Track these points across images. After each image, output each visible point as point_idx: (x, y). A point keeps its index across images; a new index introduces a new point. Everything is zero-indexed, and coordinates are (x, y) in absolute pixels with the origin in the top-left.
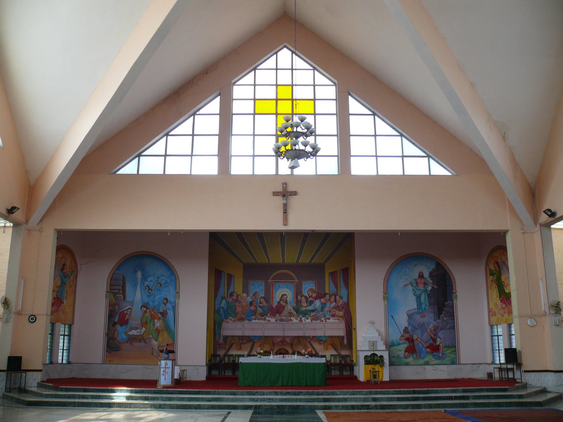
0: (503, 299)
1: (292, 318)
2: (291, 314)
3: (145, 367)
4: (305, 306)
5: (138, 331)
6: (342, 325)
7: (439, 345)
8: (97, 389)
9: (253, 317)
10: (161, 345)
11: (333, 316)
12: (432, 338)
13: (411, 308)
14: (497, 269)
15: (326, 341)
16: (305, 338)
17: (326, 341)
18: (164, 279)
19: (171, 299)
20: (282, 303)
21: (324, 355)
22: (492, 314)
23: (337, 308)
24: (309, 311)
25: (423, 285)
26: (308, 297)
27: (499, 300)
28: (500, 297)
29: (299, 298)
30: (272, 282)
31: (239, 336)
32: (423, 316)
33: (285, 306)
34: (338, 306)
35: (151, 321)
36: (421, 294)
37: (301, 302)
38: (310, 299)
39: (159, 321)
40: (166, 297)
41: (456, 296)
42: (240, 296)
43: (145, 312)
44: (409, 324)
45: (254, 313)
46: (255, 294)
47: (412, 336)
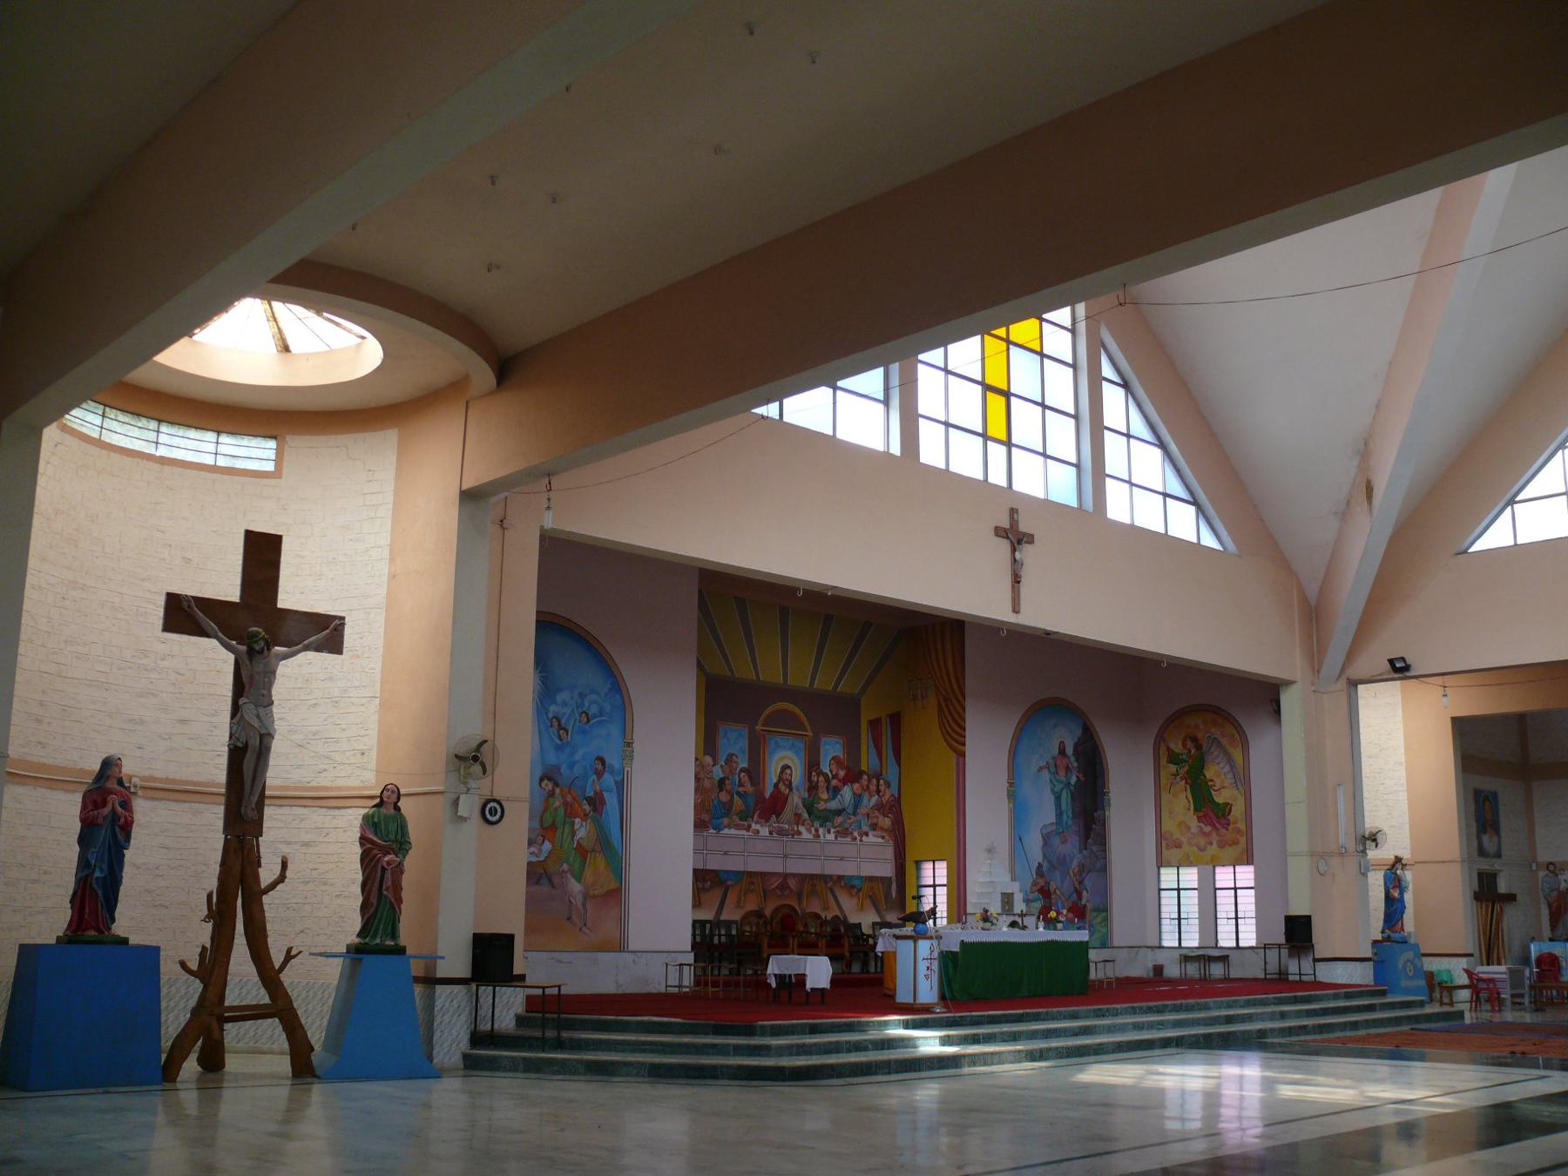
1: (802, 829)
2: (798, 817)
3: (553, 959)
4: (827, 803)
6: (889, 852)
7: (1085, 906)
8: (838, 1023)
9: (726, 821)
10: (591, 893)
11: (874, 827)
12: (1076, 890)
13: (1048, 822)
14: (1193, 751)
15: (859, 890)
16: (825, 878)
19: (613, 760)
20: (782, 787)
21: (857, 922)
23: (879, 807)
25: (1064, 771)
26: (830, 776)
27: (1195, 817)
28: (1196, 810)
30: (763, 730)
32: (1064, 842)
34: (882, 803)
35: (564, 824)
36: (1062, 791)
38: (834, 782)
39: (584, 824)
40: (602, 755)
41: (1109, 800)
43: (552, 794)
44: (1045, 856)
45: (727, 808)
47: (1049, 884)
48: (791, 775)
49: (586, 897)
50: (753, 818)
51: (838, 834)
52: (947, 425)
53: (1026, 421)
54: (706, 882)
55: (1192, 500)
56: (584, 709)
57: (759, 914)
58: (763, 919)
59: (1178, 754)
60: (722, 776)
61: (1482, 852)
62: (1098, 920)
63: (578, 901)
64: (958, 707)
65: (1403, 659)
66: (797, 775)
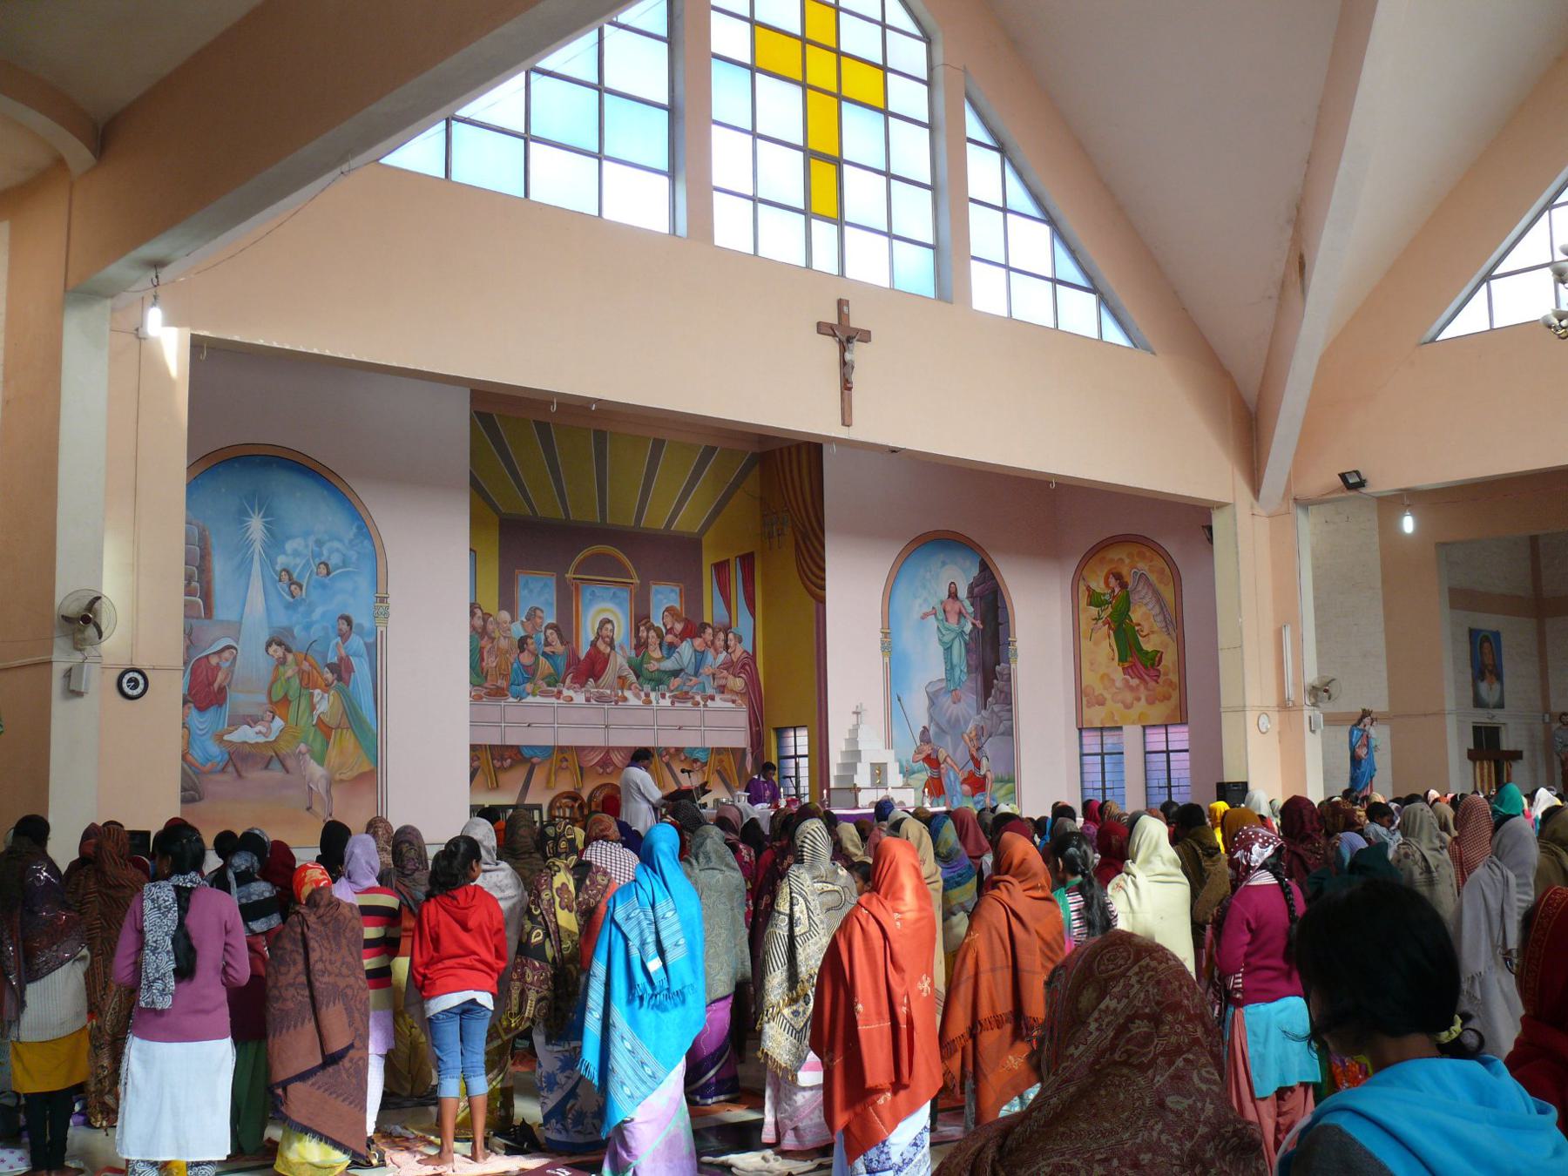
0: (1133, 666)
1: (628, 694)
4: (657, 661)
5: (259, 728)
6: (742, 718)
7: (985, 777)
9: (529, 687)
10: (338, 777)
11: (722, 689)
12: (973, 757)
14: (1117, 590)
15: (705, 764)
17: (705, 764)
18: (337, 550)
19: (361, 618)
20: (602, 646)
22: (1088, 702)
23: (728, 666)
24: (665, 672)
25: (957, 617)
26: (664, 631)
27: (1120, 669)
29: (643, 634)
31: (492, 747)
33: (609, 655)
36: (953, 640)
37: (647, 647)
38: (669, 638)
39: (326, 695)
40: (349, 612)
42: (491, 619)
43: (282, 662)
44: (931, 719)
45: (530, 673)
46: (533, 614)
48: (613, 631)
49: (330, 783)
50: (564, 683)
51: (675, 699)
52: (755, 200)
53: (863, 196)
54: (506, 760)
55: (1091, 287)
56: (323, 559)
57: (574, 796)
58: (579, 802)
59: (1100, 594)
60: (523, 634)
61: (1478, 702)
62: (1003, 792)
63: (321, 788)
64: (816, 544)
65: (1357, 473)
66: (621, 630)
